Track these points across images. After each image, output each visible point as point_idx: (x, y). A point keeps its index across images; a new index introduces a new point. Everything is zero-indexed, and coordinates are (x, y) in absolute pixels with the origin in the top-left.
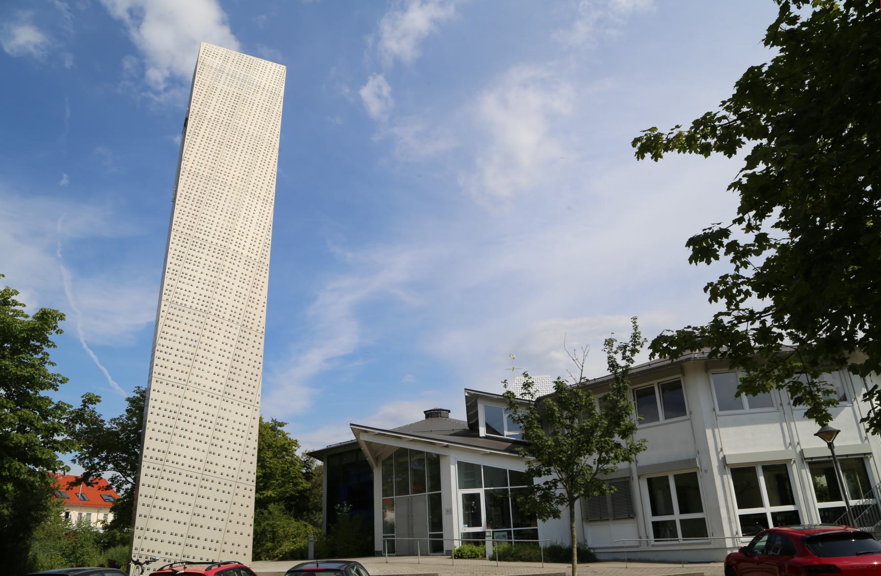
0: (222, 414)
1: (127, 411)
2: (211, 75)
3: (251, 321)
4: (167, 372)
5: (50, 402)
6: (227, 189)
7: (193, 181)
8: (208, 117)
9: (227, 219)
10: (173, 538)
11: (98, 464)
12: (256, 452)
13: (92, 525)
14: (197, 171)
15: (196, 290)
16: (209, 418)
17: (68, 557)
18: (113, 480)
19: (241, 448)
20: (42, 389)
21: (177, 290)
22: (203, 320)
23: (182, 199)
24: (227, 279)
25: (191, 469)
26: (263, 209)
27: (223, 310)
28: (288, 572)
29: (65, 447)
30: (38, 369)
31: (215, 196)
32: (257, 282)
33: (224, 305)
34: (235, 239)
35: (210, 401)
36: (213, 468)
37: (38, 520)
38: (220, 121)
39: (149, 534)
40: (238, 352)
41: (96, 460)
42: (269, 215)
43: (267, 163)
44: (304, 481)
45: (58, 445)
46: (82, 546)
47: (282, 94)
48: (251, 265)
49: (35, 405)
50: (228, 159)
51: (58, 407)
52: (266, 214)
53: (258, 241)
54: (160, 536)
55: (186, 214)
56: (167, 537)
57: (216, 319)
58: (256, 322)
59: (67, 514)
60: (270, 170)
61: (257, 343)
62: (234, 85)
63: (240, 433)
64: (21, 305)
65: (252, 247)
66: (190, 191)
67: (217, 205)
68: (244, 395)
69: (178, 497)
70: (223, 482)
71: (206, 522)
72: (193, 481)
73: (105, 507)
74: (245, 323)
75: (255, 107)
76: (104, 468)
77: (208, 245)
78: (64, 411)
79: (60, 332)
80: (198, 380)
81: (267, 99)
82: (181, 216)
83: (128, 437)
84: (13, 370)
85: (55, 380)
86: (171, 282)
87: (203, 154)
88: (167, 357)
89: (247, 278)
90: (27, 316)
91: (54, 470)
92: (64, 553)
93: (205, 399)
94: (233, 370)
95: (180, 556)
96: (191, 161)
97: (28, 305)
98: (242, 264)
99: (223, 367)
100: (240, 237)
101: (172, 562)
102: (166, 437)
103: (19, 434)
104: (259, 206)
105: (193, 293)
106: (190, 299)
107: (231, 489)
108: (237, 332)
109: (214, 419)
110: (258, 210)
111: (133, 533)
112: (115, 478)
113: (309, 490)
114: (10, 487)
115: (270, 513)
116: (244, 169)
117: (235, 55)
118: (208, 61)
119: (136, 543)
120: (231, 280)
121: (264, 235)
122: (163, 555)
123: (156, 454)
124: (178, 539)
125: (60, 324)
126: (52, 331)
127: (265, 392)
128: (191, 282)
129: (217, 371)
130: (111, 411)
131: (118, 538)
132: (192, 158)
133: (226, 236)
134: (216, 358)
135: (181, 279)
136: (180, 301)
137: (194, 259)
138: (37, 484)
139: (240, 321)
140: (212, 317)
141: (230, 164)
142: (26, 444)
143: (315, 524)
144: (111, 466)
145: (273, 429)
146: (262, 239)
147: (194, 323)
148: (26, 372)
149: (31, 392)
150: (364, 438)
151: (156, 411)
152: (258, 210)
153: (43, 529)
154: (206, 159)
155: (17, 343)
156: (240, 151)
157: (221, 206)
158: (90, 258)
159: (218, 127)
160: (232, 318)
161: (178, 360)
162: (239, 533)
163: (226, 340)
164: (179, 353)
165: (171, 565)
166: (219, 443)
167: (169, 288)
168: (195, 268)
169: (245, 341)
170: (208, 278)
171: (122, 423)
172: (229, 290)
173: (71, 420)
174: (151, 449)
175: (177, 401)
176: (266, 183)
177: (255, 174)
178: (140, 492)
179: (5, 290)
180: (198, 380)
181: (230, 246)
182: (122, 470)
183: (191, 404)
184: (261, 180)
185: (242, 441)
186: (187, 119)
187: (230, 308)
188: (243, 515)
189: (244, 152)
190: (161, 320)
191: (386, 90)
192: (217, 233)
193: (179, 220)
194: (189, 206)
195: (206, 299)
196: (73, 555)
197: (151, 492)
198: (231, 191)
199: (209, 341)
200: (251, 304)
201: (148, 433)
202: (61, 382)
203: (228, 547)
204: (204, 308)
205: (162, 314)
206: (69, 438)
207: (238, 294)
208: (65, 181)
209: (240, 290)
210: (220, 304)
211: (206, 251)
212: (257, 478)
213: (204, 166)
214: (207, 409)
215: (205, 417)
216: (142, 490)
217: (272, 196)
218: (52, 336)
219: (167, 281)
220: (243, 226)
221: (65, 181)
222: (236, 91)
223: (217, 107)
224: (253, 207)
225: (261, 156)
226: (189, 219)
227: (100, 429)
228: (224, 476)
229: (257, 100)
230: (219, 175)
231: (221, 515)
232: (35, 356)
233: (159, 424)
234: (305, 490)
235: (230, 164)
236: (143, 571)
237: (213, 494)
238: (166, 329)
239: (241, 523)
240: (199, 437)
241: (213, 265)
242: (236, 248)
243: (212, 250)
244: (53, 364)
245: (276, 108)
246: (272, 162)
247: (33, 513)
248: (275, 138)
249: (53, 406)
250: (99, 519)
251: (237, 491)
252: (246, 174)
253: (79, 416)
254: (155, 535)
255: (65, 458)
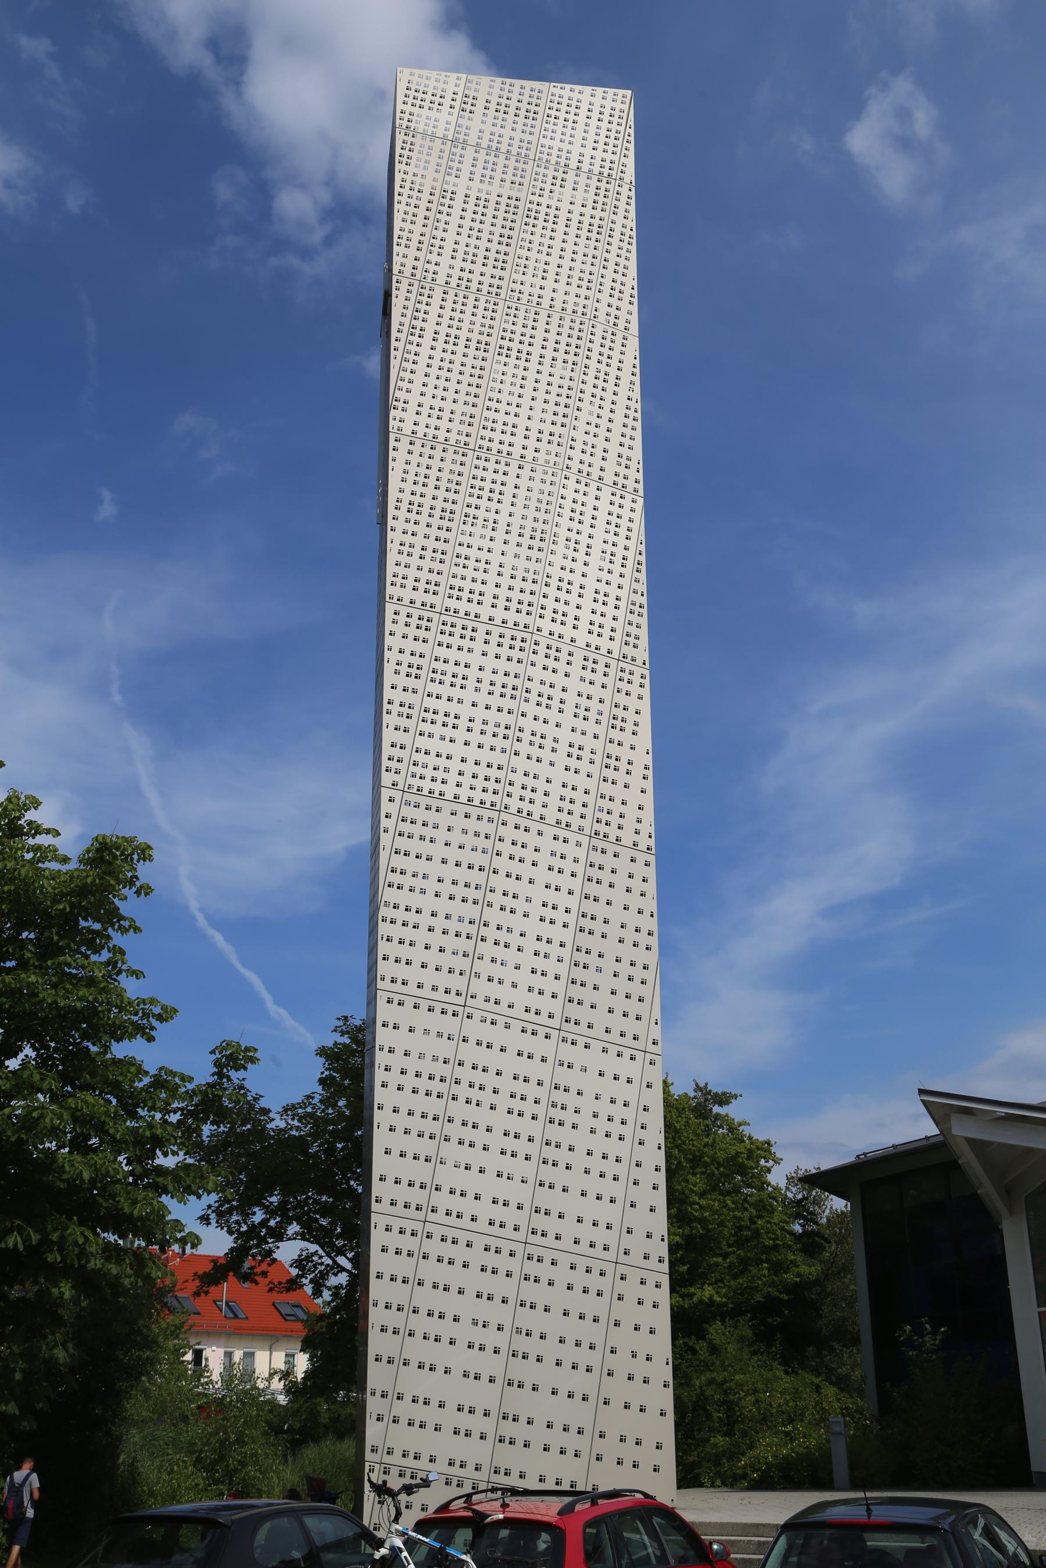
0: (563, 1077)
1: (322, 1081)
2: (434, 160)
3: (615, 819)
4: (413, 974)
5: (141, 1071)
6: (513, 470)
7: (425, 461)
8: (441, 279)
9: (524, 551)
10: (464, 1421)
11: (264, 1223)
12: (661, 1179)
13: (261, 1385)
14: (431, 432)
15: (465, 751)
16: (531, 1090)
17: (210, 1469)
18: (300, 1263)
19: (621, 1169)
20: (119, 1040)
21: (416, 757)
22: (490, 829)
23: (402, 514)
24: (542, 712)
25: (495, 1230)
26: (615, 510)
27: (539, 797)
28: (788, 1527)
29: (184, 1183)
30: (104, 990)
31: (486, 494)
32: (620, 712)
33: (541, 785)
34: (550, 604)
35: (528, 1043)
36: (551, 1224)
37: (135, 1372)
38: (474, 286)
39: (404, 1409)
40: (589, 907)
41: (259, 1216)
42: (635, 526)
43: (612, 379)
44: (799, 1258)
45: (168, 1181)
46: (240, 1441)
47: (630, 174)
48: (600, 668)
49: (106, 1081)
50: (506, 388)
51: (159, 1083)
52: (624, 523)
53: (611, 601)
54: (431, 1415)
55: (417, 552)
56: (450, 1418)
57: (523, 823)
58: (630, 824)
59: (198, 1355)
60: (622, 401)
61: (638, 878)
62: (498, 175)
63: (616, 1128)
64: (48, 831)
65: (597, 619)
66: (419, 489)
67: (492, 516)
68: (617, 1023)
69: (469, 1307)
70: (582, 1264)
71: (546, 1375)
72: (503, 1262)
73: (288, 1335)
74: (602, 828)
75: (560, 228)
76: (279, 1235)
77: (482, 629)
78: (173, 1091)
79: (145, 890)
80: (494, 990)
81: (591, 197)
82: (404, 559)
83: (330, 1151)
84: (47, 995)
85: (146, 1015)
86: (400, 737)
87: (442, 383)
88: (408, 934)
89: (594, 705)
90: (65, 860)
91: (164, 1246)
92: (199, 1460)
93: (515, 1040)
94: (582, 958)
95: (485, 1469)
96: (412, 407)
97: (64, 830)
98: (576, 670)
99: (554, 950)
100: (563, 596)
101: (467, 1489)
102: (426, 1147)
103: (77, 1157)
104: (604, 506)
105: (456, 759)
106: (453, 778)
107: (605, 1284)
108: (581, 853)
109: (542, 1093)
110: (602, 516)
111: (361, 1406)
112: (309, 1258)
113: (817, 1282)
114: (66, 1290)
115: (714, 1350)
116: (551, 408)
117: (489, 86)
118: (423, 119)
119: (373, 1432)
120: (553, 716)
121: (625, 582)
122: (441, 1466)
123: (403, 1193)
124: (477, 1424)
125: (144, 872)
126: (126, 891)
127: (670, 1013)
128: (448, 732)
129: (540, 963)
130: (285, 1085)
131: (324, 1419)
132: (414, 398)
133: (526, 598)
134: (533, 927)
135: (423, 727)
136: (427, 785)
137: (450, 668)
138: (126, 1282)
139: (586, 823)
140: (512, 820)
141: (515, 400)
142: (93, 1182)
143: (842, 1383)
144: (294, 1228)
145: (701, 1111)
146: (623, 594)
147: (470, 841)
148: (76, 999)
149: (94, 1049)
150: (962, 1129)
151: (394, 1078)
152: (602, 516)
153: (146, 1392)
154: (450, 395)
155: (49, 927)
156: (535, 359)
157: (503, 519)
158: (195, 696)
159: (471, 302)
160: (564, 817)
161: (436, 939)
162: (635, 1407)
163: (554, 878)
164: (439, 923)
165: (469, 1496)
166: (563, 1156)
167: (397, 753)
168: (456, 693)
169: (606, 876)
170: (493, 716)
171: (311, 1115)
172: (548, 743)
173: (193, 1114)
174: (390, 1180)
175: (446, 1049)
176: (615, 437)
177: (584, 416)
178: (372, 1296)
179: (9, 800)
180: (494, 990)
181: (540, 622)
182: (323, 1238)
183: (482, 1055)
184: (602, 433)
185: (622, 1149)
186: (388, 296)
187: (555, 789)
188: (641, 1356)
189: (547, 361)
190: (385, 839)
191: (924, 119)
192: (503, 593)
193: (401, 571)
194: (421, 529)
195: (493, 773)
196: (219, 1466)
197: (397, 1293)
198: (526, 473)
199: (512, 886)
200: (610, 774)
201: (380, 1139)
202: (160, 1018)
203: (610, 1448)
204: (489, 798)
205: (384, 822)
206: (190, 1161)
207: (575, 751)
208: (107, 510)
209: (577, 739)
210: (530, 782)
211: (478, 646)
212: (672, 1249)
213: (446, 415)
214: (524, 1067)
215: (520, 1087)
216: (378, 1290)
217: (635, 474)
218: (128, 905)
219: (388, 736)
220: (569, 564)
221: (107, 510)
222: (506, 192)
223: (461, 248)
224: (589, 511)
225: (593, 364)
226: (426, 564)
227: (260, 1132)
228: (584, 1248)
229: (565, 206)
230: (488, 434)
231: (584, 1356)
232: (94, 958)
233: (404, 1111)
234: (799, 1290)
235: (515, 400)
236: (398, 1514)
237: (558, 1297)
238: (398, 862)
239: (639, 1379)
240: (510, 1144)
241: (499, 679)
242: (557, 628)
243: (494, 639)
244: (137, 974)
245: (619, 219)
246: (626, 376)
247: (120, 1354)
248: (624, 305)
249: (147, 1080)
250: (275, 1365)
251: (621, 1287)
252: (559, 419)
253: (209, 1103)
254: (419, 1412)
255: (185, 1211)
